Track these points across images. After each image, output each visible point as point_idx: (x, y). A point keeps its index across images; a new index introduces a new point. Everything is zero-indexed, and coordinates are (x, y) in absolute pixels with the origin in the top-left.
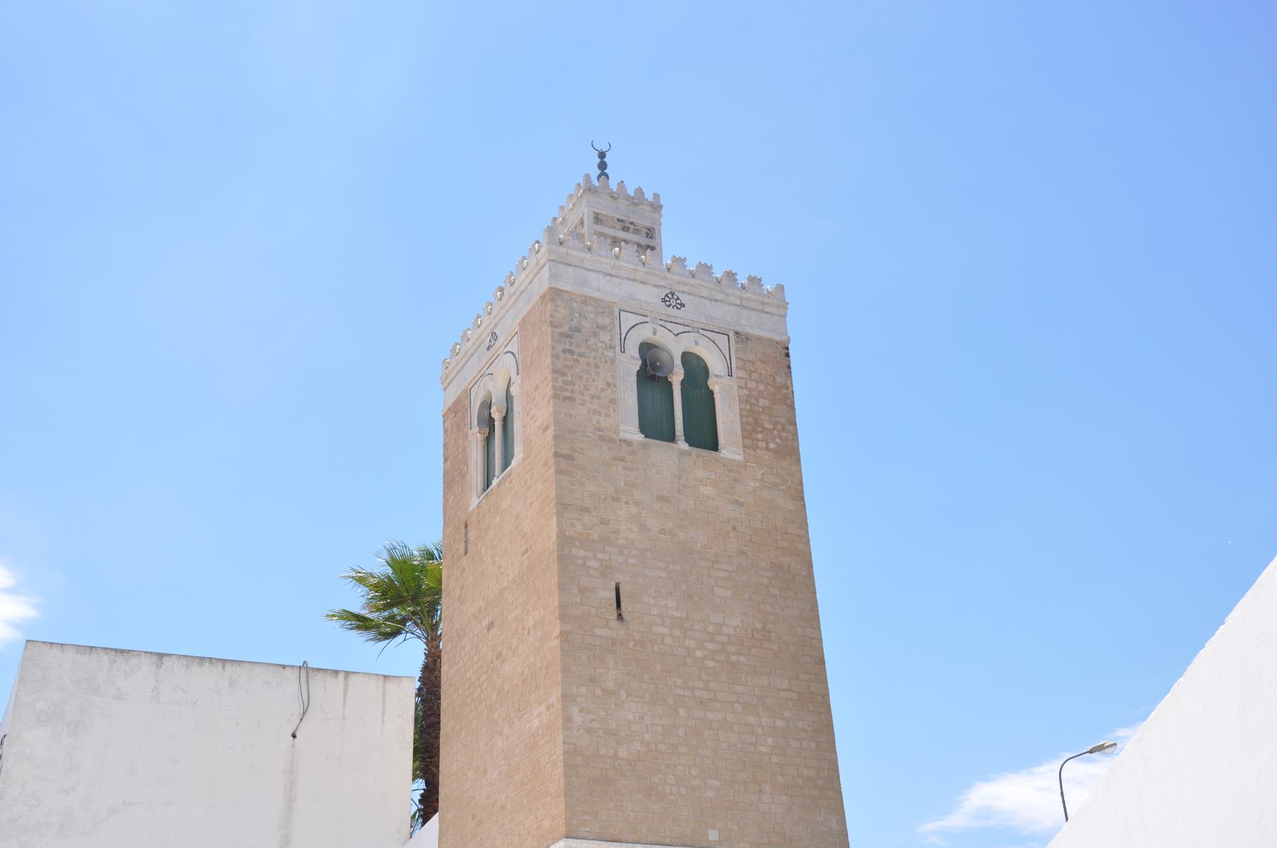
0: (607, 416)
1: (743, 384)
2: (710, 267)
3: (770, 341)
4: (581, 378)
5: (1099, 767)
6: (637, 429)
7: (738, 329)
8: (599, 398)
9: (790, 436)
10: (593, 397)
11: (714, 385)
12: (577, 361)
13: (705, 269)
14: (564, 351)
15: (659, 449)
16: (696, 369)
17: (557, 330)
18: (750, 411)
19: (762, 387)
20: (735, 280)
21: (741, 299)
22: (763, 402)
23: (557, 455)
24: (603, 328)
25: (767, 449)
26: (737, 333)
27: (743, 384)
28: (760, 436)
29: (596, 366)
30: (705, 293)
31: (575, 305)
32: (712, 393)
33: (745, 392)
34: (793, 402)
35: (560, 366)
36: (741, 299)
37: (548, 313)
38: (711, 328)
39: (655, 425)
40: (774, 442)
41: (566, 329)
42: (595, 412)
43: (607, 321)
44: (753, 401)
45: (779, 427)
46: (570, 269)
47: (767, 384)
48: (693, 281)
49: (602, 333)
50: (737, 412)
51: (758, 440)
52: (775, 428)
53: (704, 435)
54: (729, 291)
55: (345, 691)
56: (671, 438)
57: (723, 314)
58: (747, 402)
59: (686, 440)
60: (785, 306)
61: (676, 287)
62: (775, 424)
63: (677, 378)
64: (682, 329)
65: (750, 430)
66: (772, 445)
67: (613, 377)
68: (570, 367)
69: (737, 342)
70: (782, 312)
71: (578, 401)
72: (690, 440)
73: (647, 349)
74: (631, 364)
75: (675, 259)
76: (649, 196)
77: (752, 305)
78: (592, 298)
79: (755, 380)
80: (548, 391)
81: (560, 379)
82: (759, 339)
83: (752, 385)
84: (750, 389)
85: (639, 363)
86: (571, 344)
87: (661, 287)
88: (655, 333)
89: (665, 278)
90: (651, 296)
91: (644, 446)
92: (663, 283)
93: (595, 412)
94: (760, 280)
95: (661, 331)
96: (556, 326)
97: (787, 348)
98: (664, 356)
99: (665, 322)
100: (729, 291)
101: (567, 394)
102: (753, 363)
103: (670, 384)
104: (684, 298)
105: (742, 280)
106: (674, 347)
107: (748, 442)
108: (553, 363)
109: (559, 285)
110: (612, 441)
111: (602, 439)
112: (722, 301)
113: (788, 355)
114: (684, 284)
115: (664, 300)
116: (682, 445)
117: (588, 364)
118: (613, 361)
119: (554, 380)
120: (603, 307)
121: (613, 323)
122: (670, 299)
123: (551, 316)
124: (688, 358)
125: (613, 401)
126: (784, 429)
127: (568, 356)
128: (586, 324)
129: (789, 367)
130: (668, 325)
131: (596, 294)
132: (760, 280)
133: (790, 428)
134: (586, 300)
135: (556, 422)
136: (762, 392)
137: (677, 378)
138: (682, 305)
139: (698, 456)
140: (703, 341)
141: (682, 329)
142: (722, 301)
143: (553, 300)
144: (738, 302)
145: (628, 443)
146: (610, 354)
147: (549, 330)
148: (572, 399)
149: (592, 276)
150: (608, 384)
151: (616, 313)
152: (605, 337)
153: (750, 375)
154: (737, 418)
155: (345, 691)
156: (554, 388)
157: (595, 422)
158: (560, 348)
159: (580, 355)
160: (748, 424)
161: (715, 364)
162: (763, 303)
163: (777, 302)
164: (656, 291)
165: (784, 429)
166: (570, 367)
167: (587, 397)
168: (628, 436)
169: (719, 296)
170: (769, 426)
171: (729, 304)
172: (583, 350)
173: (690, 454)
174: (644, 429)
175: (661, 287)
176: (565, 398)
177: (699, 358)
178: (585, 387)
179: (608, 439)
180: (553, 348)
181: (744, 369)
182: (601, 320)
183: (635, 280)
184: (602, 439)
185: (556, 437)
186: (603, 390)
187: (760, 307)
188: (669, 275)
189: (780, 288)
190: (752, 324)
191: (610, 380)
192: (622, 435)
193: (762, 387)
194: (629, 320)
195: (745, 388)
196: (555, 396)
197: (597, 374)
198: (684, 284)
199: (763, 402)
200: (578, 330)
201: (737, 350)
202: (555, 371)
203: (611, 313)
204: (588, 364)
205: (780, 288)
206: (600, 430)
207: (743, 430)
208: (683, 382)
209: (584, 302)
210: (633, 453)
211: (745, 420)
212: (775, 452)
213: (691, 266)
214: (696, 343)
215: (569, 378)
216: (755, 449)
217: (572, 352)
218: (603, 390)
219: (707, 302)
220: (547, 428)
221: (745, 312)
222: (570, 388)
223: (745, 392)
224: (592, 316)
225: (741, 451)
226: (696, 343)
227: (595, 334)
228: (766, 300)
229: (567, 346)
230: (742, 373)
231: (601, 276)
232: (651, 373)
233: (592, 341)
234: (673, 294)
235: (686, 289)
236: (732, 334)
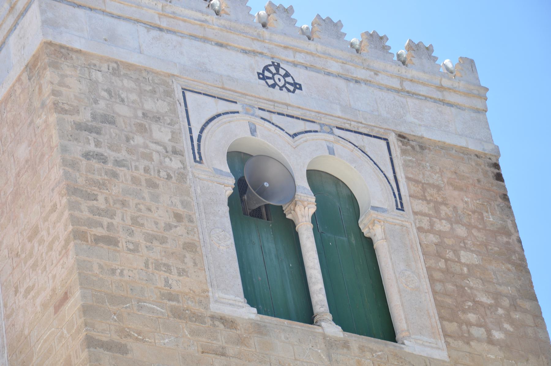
0: (182, 272)
1: (425, 223)
2: (338, 25)
3: (464, 152)
4: (124, 204)
5: (343, 28)
6: (241, 299)
7: (403, 129)
8: (163, 240)
9: (529, 320)
10: (151, 238)
11: (373, 226)
12: (115, 175)
13: (330, 27)
14: (87, 156)
15: (286, 333)
16: (338, 207)
17: (69, 118)
18: (446, 271)
19: (461, 231)
20: (386, 49)
21: (402, 79)
22: (466, 257)
23: (91, 342)
24: (157, 119)
25: (491, 341)
26: (401, 137)
27: (425, 223)
28: (472, 317)
29: (152, 184)
30: (335, 67)
31: (98, 76)
32: (369, 242)
33: (433, 238)
34: (523, 259)
35: (81, 181)
36: (402, 79)
37: (47, 90)
38: (354, 126)
40: (501, 329)
41: (85, 116)
42: (158, 266)
43: (161, 106)
44: (450, 255)
45: (506, 302)
46: (80, 12)
47: (469, 226)
48: (312, 46)
49: (155, 127)
50: (423, 272)
51: (469, 324)
52: (497, 305)
54: (378, 64)
57: (368, 104)
58: (439, 256)
59: (337, 320)
60: (482, 93)
61: (282, 56)
62: (497, 296)
63: (303, 212)
64: (301, 126)
65: (452, 309)
66: (497, 335)
67: (185, 204)
68: (101, 185)
69: (404, 152)
70: (478, 104)
71: (122, 244)
75: (272, 9)
76: (343, 30)
77: (423, 90)
78: (129, 66)
79: (448, 219)
80: (62, 229)
81: (85, 205)
82: (444, 148)
83: (443, 226)
84: (440, 233)
85: (231, 181)
86: (98, 144)
87: (255, 53)
88: (253, 131)
89: (259, 39)
90: (240, 69)
91: (259, 329)
92: (256, 46)
93: (158, 266)
94: (429, 49)
95: (263, 128)
96: (65, 112)
97: (496, 166)
98: (272, 172)
99: (269, 113)
100: (378, 64)
101: (100, 232)
102: (439, 188)
103: (290, 229)
104: (299, 75)
105: (399, 48)
106: (296, 156)
107: (452, 327)
108: (66, 175)
109: (64, 39)
110: (198, 318)
111: (178, 314)
112: (367, 82)
113: (499, 177)
114: (296, 51)
115: (262, 76)
116: (333, 330)
117: (135, 180)
118: (182, 177)
119: (73, 206)
120: (152, 82)
121: (174, 111)
122: (271, 74)
123: (54, 93)
124: (314, 177)
125: (190, 247)
126: (514, 306)
127: (96, 164)
128: (122, 110)
129: (505, 198)
130: (275, 118)
131: (135, 59)
132: (429, 49)
133: (527, 305)
134: (118, 68)
135: (85, 281)
136: (463, 240)
137: (303, 212)
138: (297, 86)
139: (362, 349)
140: (342, 148)
141: (301, 126)
142: (367, 82)
143: (55, 65)
144: (395, 83)
145: (229, 323)
146: (175, 164)
147: (53, 118)
148: (111, 241)
149: (123, 27)
150: (178, 217)
151: (179, 95)
152: (162, 134)
153: (437, 210)
154: (426, 284)
156: (74, 220)
157: (161, 284)
158: (77, 150)
159: (118, 163)
160: (446, 294)
161: (369, 187)
162: (441, 88)
163: (468, 88)
164: (247, 60)
165: (514, 306)
166: (101, 185)
167: (139, 238)
168: (227, 311)
169: (361, 74)
170: (486, 300)
171: (380, 87)
172: (123, 155)
173: (346, 345)
174: (252, 298)
175: (255, 53)
176: (97, 239)
177: (337, 181)
178: (135, 221)
179: (185, 313)
180: (64, 149)
181: (424, 198)
182: (149, 105)
183: (205, 40)
184: (178, 314)
185: (86, 310)
186: (169, 227)
187: (438, 95)
188: (266, 33)
189: (469, 64)
191: (180, 209)
192: (215, 308)
193: (461, 231)
194: (202, 108)
195: (431, 230)
196: (79, 235)
197: (155, 198)
198: (296, 51)
199: (466, 257)
200: (108, 119)
201: (406, 165)
202: (73, 190)
203: (169, 93)
204: (135, 180)
205: (469, 64)
206: (171, 297)
207: (439, 305)
208: (315, 219)
209: (115, 72)
210: (240, 341)
211: (439, 287)
212: (505, 346)
213: (304, 23)
214: (331, 152)
215: (101, 203)
216: (468, 339)
217: (103, 159)
218: (169, 227)
219: (341, 83)
220: (66, 297)
221: (411, 102)
222: (106, 221)
223: (433, 238)
224: (133, 97)
225: (441, 343)
226: (331, 152)
227: (142, 129)
228: (446, 83)
229: (92, 147)
230: (420, 206)
231: (142, 29)
232: (254, 205)
233: (139, 140)
234: (277, 67)
235: (300, 58)
236: (392, 138)
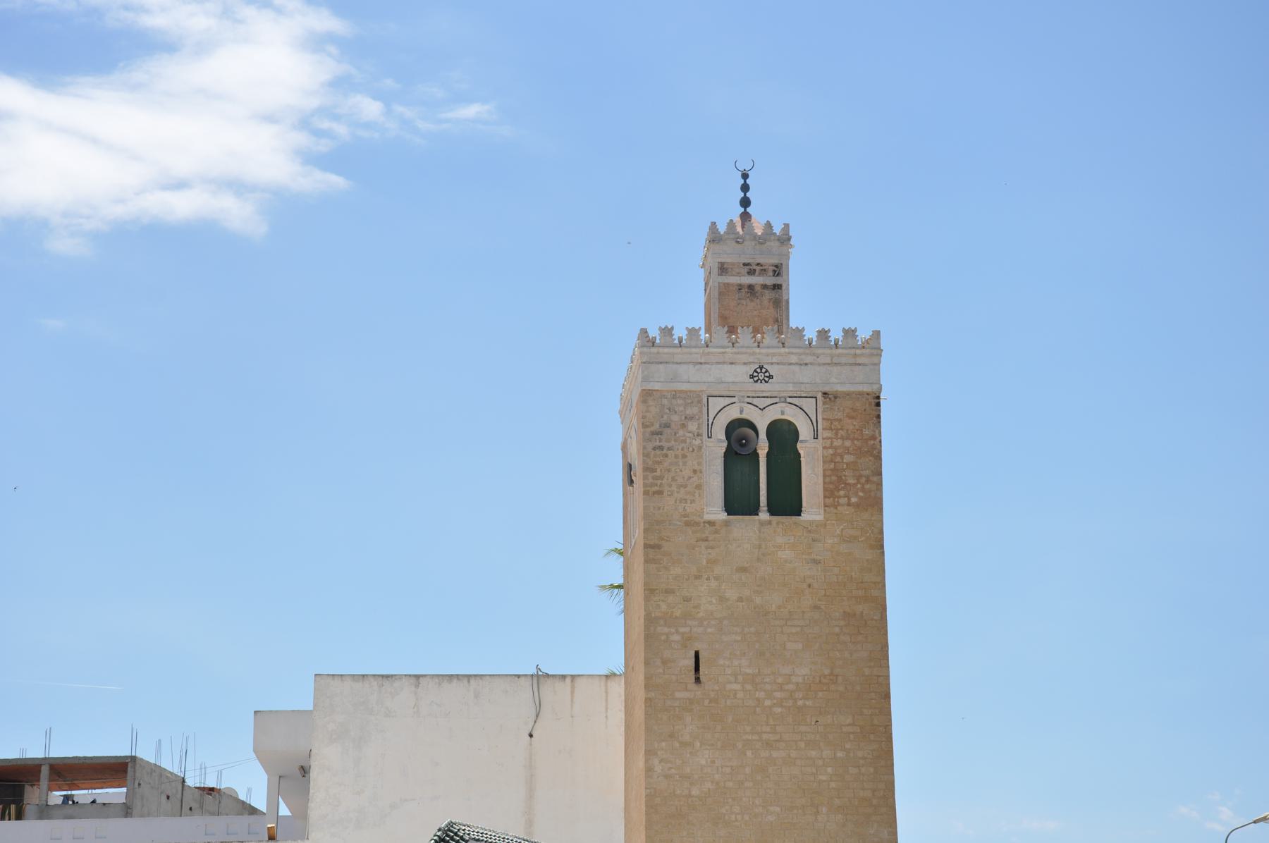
16: (783, 435)
39: (739, 502)
53: (787, 501)
55: (572, 692)
56: (754, 511)
63: (763, 449)
72: (773, 510)
73: (739, 432)
74: (717, 447)
90: (740, 374)
120: (696, 399)
122: (761, 374)
134: (675, 395)
155: (572, 692)
190: (840, 381)
